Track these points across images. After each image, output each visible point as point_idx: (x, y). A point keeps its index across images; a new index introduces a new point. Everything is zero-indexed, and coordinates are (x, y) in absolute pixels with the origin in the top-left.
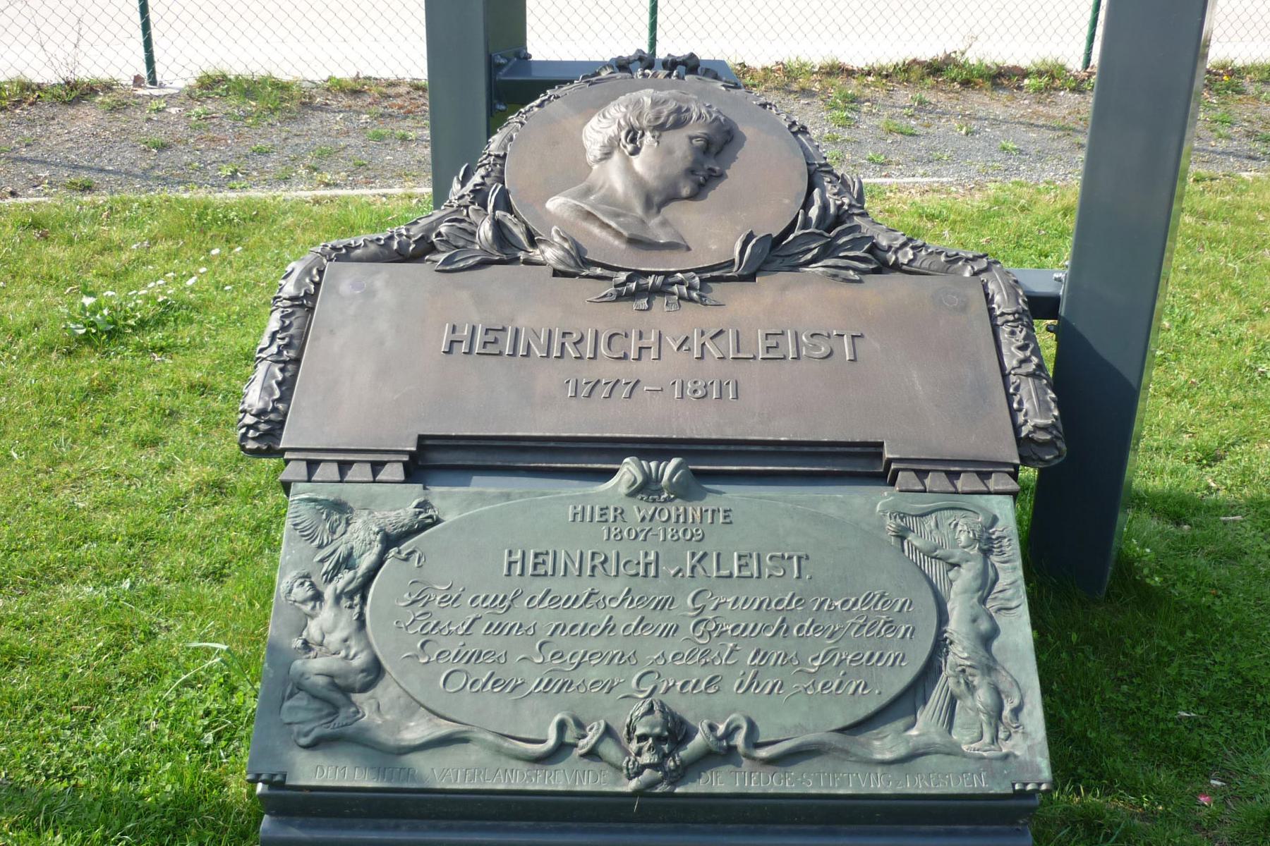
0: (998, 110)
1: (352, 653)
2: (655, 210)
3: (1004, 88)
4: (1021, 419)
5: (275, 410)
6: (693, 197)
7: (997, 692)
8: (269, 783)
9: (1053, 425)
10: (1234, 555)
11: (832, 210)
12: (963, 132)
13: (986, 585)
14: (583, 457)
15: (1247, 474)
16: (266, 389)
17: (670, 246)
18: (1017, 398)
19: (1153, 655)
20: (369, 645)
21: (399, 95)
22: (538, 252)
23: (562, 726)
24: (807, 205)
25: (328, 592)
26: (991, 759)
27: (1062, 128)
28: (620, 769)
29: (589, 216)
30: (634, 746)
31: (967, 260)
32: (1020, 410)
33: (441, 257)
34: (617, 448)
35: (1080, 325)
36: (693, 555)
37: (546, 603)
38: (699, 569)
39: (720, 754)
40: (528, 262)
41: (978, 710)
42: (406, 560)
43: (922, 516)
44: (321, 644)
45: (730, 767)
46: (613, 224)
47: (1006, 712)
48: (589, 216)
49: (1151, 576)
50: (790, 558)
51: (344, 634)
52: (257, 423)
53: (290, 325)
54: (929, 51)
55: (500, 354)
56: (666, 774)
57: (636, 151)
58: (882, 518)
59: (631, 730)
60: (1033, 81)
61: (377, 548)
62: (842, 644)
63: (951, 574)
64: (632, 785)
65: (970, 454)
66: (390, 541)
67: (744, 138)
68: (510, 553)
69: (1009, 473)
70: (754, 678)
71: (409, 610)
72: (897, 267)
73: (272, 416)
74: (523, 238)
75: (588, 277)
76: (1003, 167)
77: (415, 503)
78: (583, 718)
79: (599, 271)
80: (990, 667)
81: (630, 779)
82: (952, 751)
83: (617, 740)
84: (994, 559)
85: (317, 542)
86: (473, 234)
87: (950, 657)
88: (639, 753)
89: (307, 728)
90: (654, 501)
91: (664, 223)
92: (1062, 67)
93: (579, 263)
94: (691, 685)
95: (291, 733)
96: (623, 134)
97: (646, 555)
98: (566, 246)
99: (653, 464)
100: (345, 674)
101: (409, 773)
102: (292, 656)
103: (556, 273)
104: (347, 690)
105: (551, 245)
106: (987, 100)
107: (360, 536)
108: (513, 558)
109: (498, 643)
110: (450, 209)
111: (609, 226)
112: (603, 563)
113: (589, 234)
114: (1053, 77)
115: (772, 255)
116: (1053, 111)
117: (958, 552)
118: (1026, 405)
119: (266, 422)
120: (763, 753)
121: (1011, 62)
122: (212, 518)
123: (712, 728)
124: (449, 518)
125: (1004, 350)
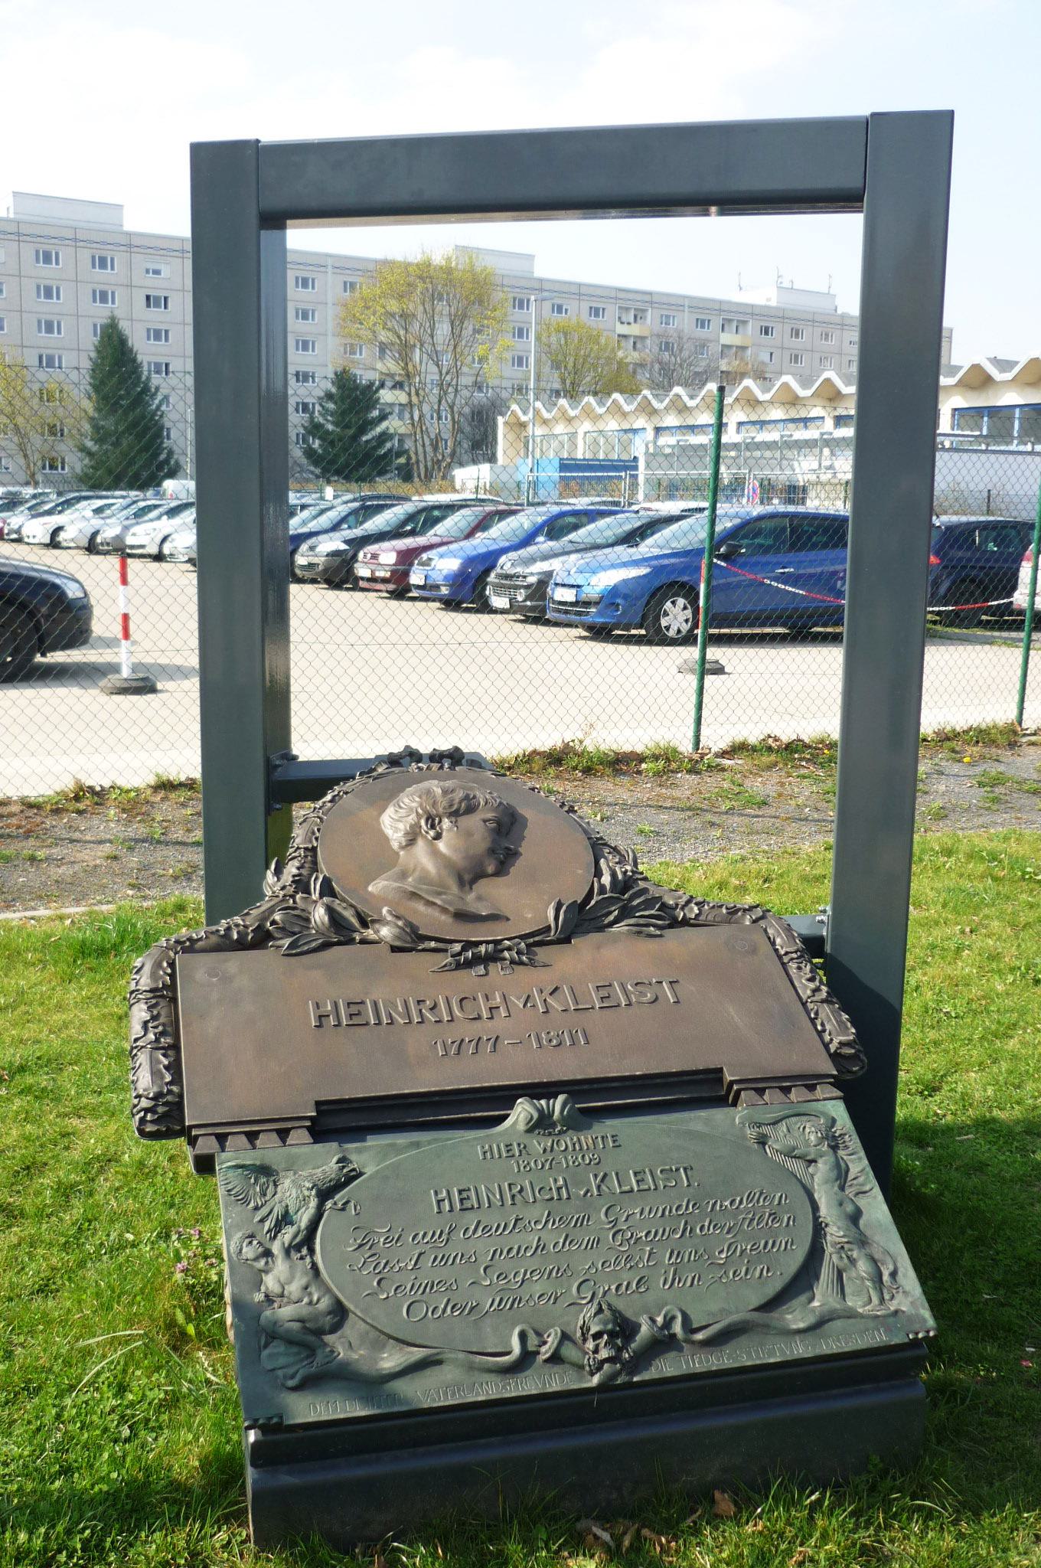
0: (624, 795)
1: (315, 1298)
2: (467, 887)
3: (624, 774)
4: (827, 1038)
5: (170, 1092)
6: (498, 873)
7: (873, 1261)
8: (264, 1429)
9: (854, 1041)
10: (980, 1167)
11: (620, 877)
12: (598, 818)
13: (841, 1175)
14: (475, 1107)
15: (965, 1099)
16: (155, 1074)
17: (494, 917)
18: (818, 1022)
19: (946, 1252)
20: (328, 1290)
21: (11, 815)
22: (370, 931)
23: (523, 1336)
24: (598, 873)
25: (276, 1248)
26: (884, 1316)
27: (689, 809)
28: (582, 1367)
29: (414, 895)
30: (590, 1345)
31: (745, 910)
32: (824, 1031)
33: (287, 942)
34: (504, 1097)
35: (846, 959)
36: (596, 1176)
37: (479, 1233)
38: (603, 1187)
39: (663, 1343)
40: (363, 942)
41: (863, 1278)
42: (343, 1209)
43: (774, 1124)
44: (282, 1296)
45: (673, 1354)
46: (439, 902)
47: (886, 1277)
48: (414, 895)
49: (925, 1185)
50: (677, 1170)
51: (304, 1281)
52: (156, 1106)
53: (159, 1014)
54: (547, 741)
55: (367, 1024)
56: (623, 1365)
57: (438, 837)
58: (742, 1129)
59: (585, 1329)
60: (651, 765)
61: (313, 1203)
62: (739, 1237)
63: (811, 1170)
64: (596, 1380)
65: (796, 1070)
66: (325, 1194)
67: (526, 820)
68: (436, 1193)
69: (307, 1128)
70: (675, 1274)
71: (357, 1254)
72: (685, 922)
73: (169, 1098)
74: (354, 921)
75: (424, 950)
76: (646, 849)
77: (335, 1159)
78: (539, 1327)
79: (433, 944)
80: (863, 1242)
81: (592, 1374)
82: (851, 1315)
83: (574, 1342)
84: (841, 1153)
85: (252, 1205)
86: (308, 920)
87: (828, 1238)
88: (596, 1351)
89: (291, 1371)
90: (550, 1134)
91: (479, 898)
92: (675, 750)
93: (412, 940)
94: (624, 1287)
95: (277, 1377)
96: (423, 822)
97: (556, 1181)
98: (400, 923)
99: (543, 1102)
100: (315, 1317)
101: (393, 1398)
102: (259, 1309)
103: (394, 949)
104: (319, 1332)
105: (386, 923)
106: (611, 786)
107: (293, 1192)
108: (440, 1197)
109: (445, 1273)
110: (276, 900)
111: (434, 904)
112: (520, 1192)
113: (415, 912)
114: (668, 760)
115: (582, 919)
116: (676, 793)
117: (812, 1150)
118: (828, 1027)
119: (164, 1104)
120: (700, 1336)
121: (627, 748)
122: (15, 1240)
123: (653, 1321)
124: (369, 1171)
125: (796, 984)
